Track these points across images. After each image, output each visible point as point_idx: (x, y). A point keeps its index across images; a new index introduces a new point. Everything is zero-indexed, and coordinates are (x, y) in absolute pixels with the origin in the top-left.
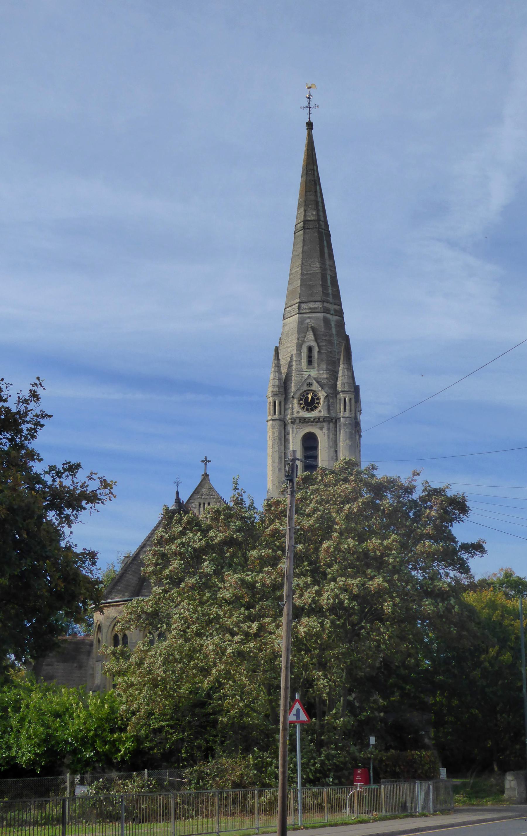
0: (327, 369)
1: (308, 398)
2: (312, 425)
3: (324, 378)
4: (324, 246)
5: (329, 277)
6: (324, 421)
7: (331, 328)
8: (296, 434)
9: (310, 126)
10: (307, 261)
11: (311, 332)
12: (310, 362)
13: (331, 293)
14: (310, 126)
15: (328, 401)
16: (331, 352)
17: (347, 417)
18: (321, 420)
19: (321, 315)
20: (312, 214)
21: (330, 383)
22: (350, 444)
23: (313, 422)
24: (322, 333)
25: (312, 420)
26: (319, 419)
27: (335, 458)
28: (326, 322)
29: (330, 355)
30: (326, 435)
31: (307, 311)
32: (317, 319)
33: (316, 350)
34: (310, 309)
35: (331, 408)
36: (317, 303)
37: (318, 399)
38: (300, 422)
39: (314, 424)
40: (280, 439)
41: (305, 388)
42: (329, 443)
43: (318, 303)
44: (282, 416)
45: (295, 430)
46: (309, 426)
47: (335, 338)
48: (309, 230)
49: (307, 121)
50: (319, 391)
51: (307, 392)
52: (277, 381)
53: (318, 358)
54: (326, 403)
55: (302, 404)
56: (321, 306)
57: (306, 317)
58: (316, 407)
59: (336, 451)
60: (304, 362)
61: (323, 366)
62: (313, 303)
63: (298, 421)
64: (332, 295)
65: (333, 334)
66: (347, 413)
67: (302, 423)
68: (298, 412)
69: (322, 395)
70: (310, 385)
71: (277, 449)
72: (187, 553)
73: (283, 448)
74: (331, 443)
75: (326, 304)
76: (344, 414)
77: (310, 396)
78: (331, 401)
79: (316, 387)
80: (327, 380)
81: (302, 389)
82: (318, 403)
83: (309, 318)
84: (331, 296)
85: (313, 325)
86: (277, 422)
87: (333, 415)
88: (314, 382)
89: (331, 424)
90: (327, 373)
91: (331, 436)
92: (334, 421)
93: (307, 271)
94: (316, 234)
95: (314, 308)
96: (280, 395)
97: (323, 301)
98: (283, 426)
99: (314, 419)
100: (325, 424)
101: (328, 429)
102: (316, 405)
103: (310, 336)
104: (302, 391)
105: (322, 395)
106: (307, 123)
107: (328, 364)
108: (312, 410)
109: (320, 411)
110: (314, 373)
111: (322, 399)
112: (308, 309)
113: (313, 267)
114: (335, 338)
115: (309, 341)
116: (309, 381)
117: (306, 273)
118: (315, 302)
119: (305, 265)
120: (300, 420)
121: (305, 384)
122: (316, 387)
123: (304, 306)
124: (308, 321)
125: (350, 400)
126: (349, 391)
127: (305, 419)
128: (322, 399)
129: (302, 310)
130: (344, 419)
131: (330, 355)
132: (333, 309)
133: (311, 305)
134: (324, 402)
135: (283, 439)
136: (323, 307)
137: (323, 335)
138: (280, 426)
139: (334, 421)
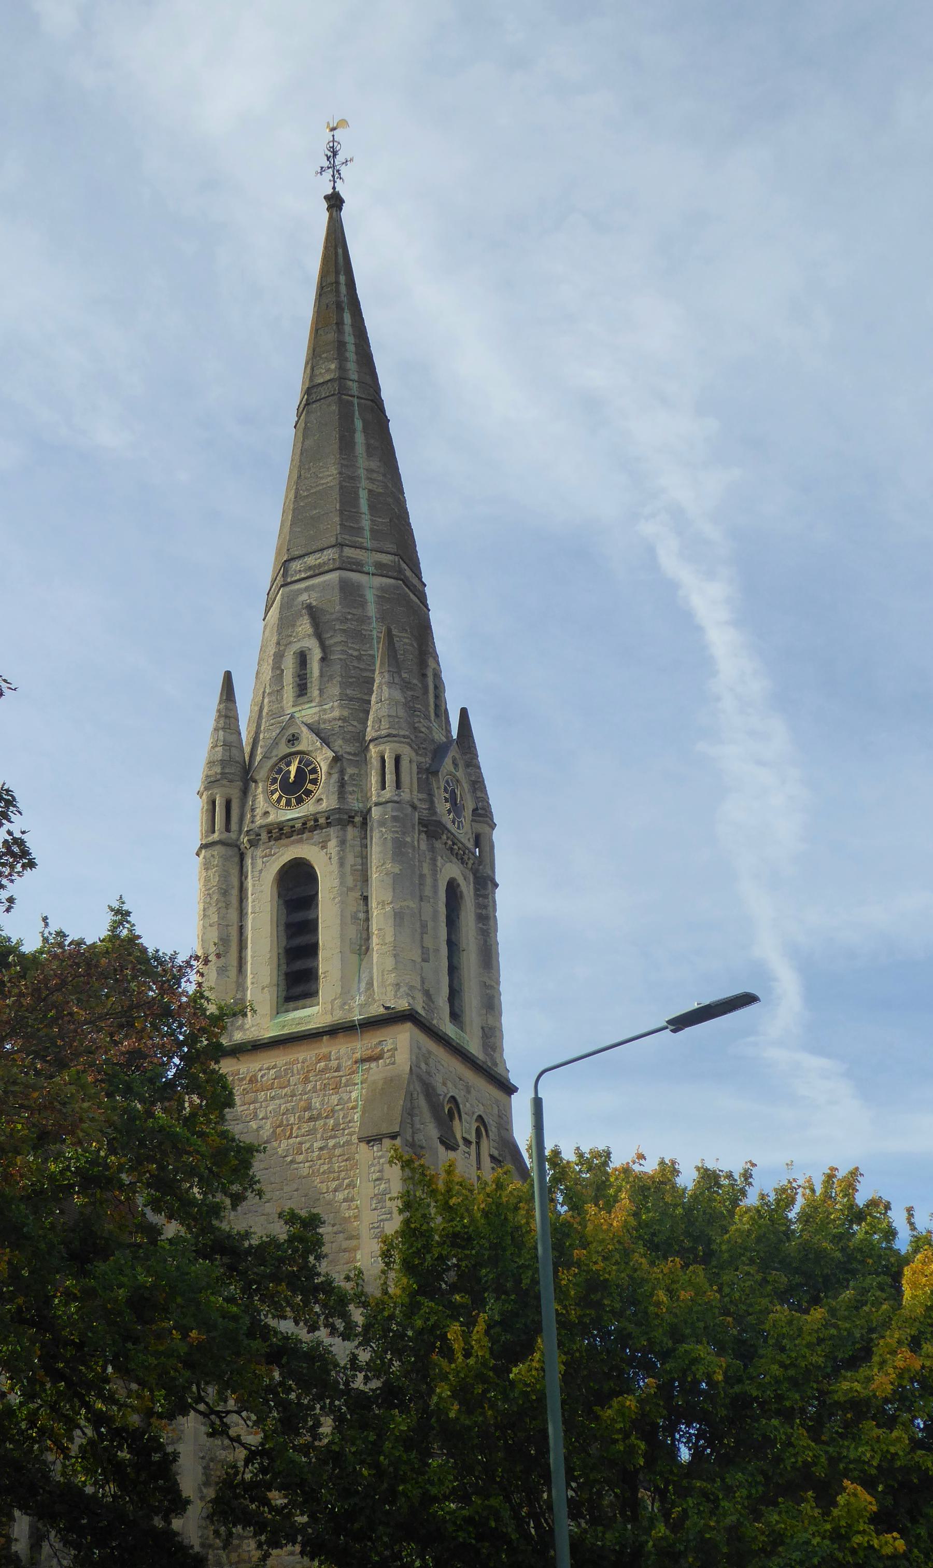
0: (343, 697)
1: (289, 772)
2: (300, 841)
3: (335, 719)
4: (353, 431)
5: (363, 495)
6: (329, 825)
7: (363, 604)
8: (261, 871)
9: (335, 202)
10: (309, 469)
11: (306, 617)
12: (302, 689)
13: (367, 528)
14: (335, 202)
15: (342, 772)
16: (359, 658)
17: (387, 802)
18: (322, 821)
19: (334, 576)
20: (328, 370)
21: (350, 728)
22: (397, 870)
23: (302, 831)
24: (334, 617)
25: (298, 825)
26: (316, 820)
27: (361, 916)
28: (350, 592)
29: (355, 664)
30: (335, 859)
31: (303, 575)
32: (324, 587)
33: (316, 655)
34: (310, 568)
35: (349, 789)
36: (325, 552)
37: (314, 771)
38: (270, 838)
39: (305, 836)
40: (225, 893)
41: (284, 749)
42: (342, 876)
43: (330, 550)
44: (233, 835)
45: (259, 861)
46: (293, 843)
47: (374, 625)
48: (318, 404)
49: (330, 191)
50: (316, 750)
51: (287, 759)
52: (219, 749)
53: (322, 675)
54: (335, 777)
55: (276, 790)
56: (336, 556)
57: (298, 590)
58: (308, 793)
59: (366, 899)
60: (289, 692)
61: (334, 690)
62: (317, 555)
63: (264, 836)
64: (372, 530)
65: (369, 618)
66: (388, 793)
67: (277, 839)
68: (266, 813)
69: (322, 759)
70: (294, 739)
71: (215, 918)
72: (802, 1398)
73: (233, 915)
74: (350, 881)
75: (348, 551)
76: (379, 796)
77: (293, 769)
78: (350, 771)
79: (308, 741)
80: (340, 723)
81: (274, 753)
82: (314, 782)
83: (307, 589)
84: (367, 534)
85: (314, 603)
86: (217, 851)
87: (355, 804)
88: (305, 729)
89: (350, 829)
90: (341, 706)
91: (350, 859)
92: (358, 819)
93: (307, 490)
94: (334, 408)
95: (320, 565)
96: (225, 782)
97: (341, 545)
98: (237, 859)
99: (304, 824)
100: (332, 831)
101: (342, 843)
102: (310, 787)
103: (305, 626)
104: (274, 759)
105: (322, 759)
106: (327, 198)
107: (344, 685)
108: (300, 801)
109: (320, 800)
110: (308, 712)
111: (324, 767)
112: (305, 571)
113: (322, 478)
114: (374, 625)
115: (299, 640)
116: (291, 731)
117: (306, 494)
118: (322, 550)
119: (306, 478)
120: (270, 832)
121: (284, 740)
122: (308, 741)
123: (296, 566)
124: (304, 597)
125: (397, 760)
126: (389, 735)
127: (280, 826)
128: (324, 767)
129: (292, 576)
130: (379, 808)
131: (355, 664)
132: (371, 561)
133: (311, 560)
134: (329, 774)
135: (235, 892)
136: (341, 556)
137: (337, 619)
138: (225, 858)
139: (358, 819)
